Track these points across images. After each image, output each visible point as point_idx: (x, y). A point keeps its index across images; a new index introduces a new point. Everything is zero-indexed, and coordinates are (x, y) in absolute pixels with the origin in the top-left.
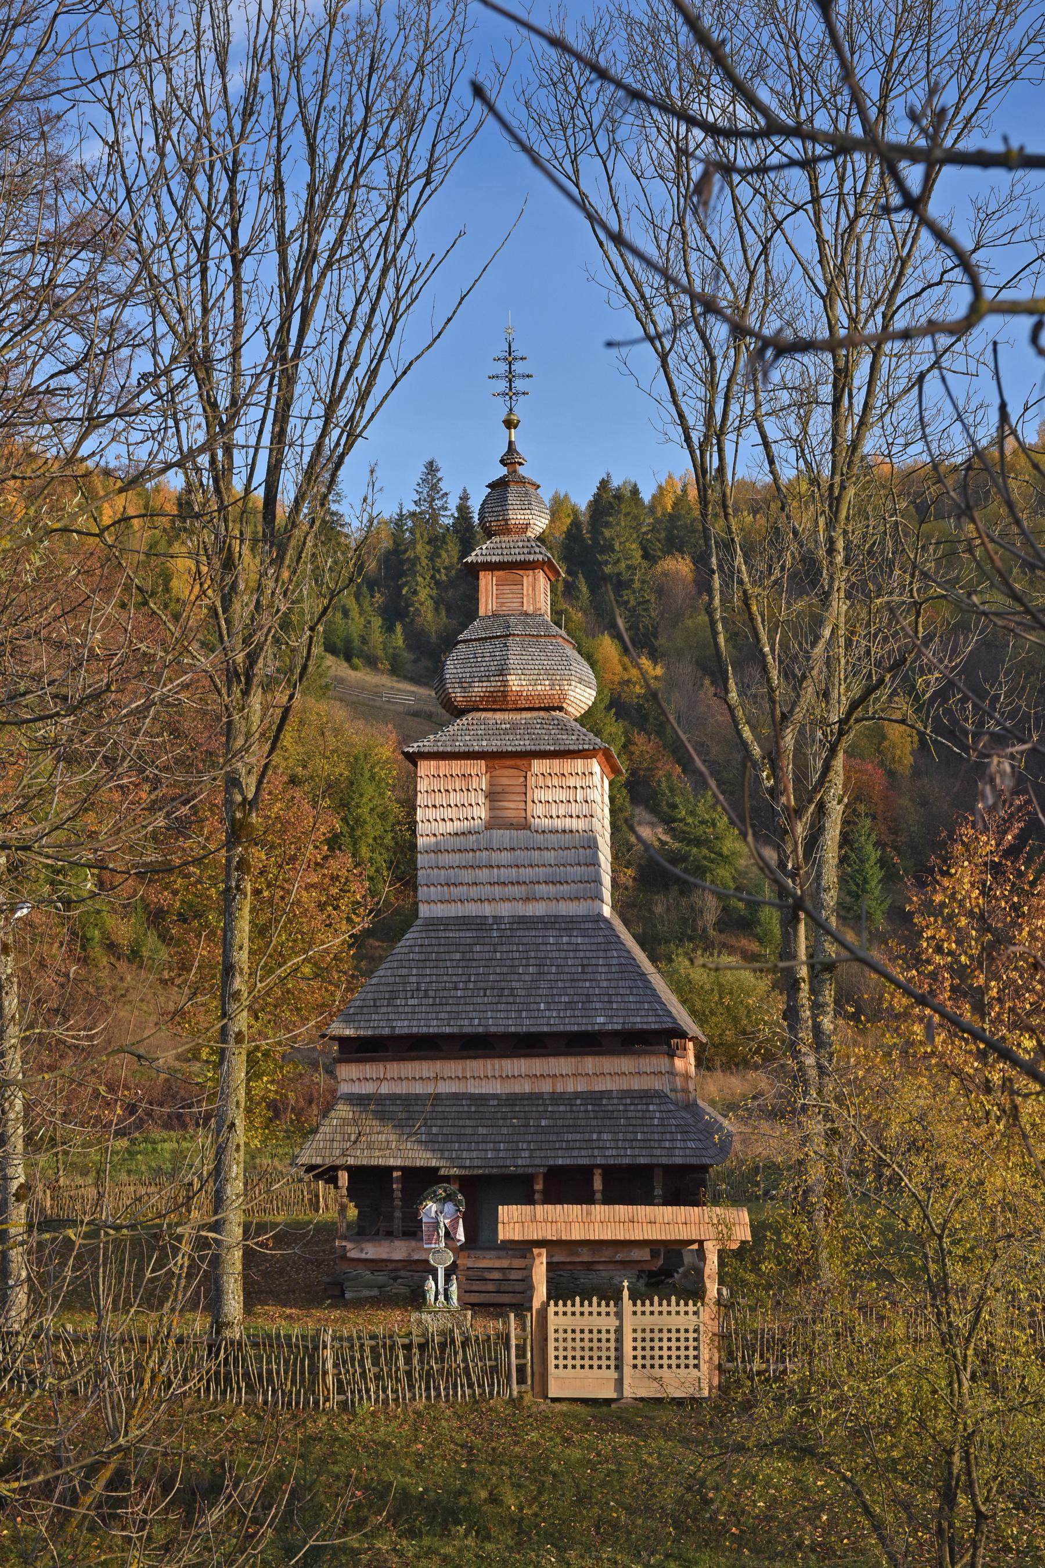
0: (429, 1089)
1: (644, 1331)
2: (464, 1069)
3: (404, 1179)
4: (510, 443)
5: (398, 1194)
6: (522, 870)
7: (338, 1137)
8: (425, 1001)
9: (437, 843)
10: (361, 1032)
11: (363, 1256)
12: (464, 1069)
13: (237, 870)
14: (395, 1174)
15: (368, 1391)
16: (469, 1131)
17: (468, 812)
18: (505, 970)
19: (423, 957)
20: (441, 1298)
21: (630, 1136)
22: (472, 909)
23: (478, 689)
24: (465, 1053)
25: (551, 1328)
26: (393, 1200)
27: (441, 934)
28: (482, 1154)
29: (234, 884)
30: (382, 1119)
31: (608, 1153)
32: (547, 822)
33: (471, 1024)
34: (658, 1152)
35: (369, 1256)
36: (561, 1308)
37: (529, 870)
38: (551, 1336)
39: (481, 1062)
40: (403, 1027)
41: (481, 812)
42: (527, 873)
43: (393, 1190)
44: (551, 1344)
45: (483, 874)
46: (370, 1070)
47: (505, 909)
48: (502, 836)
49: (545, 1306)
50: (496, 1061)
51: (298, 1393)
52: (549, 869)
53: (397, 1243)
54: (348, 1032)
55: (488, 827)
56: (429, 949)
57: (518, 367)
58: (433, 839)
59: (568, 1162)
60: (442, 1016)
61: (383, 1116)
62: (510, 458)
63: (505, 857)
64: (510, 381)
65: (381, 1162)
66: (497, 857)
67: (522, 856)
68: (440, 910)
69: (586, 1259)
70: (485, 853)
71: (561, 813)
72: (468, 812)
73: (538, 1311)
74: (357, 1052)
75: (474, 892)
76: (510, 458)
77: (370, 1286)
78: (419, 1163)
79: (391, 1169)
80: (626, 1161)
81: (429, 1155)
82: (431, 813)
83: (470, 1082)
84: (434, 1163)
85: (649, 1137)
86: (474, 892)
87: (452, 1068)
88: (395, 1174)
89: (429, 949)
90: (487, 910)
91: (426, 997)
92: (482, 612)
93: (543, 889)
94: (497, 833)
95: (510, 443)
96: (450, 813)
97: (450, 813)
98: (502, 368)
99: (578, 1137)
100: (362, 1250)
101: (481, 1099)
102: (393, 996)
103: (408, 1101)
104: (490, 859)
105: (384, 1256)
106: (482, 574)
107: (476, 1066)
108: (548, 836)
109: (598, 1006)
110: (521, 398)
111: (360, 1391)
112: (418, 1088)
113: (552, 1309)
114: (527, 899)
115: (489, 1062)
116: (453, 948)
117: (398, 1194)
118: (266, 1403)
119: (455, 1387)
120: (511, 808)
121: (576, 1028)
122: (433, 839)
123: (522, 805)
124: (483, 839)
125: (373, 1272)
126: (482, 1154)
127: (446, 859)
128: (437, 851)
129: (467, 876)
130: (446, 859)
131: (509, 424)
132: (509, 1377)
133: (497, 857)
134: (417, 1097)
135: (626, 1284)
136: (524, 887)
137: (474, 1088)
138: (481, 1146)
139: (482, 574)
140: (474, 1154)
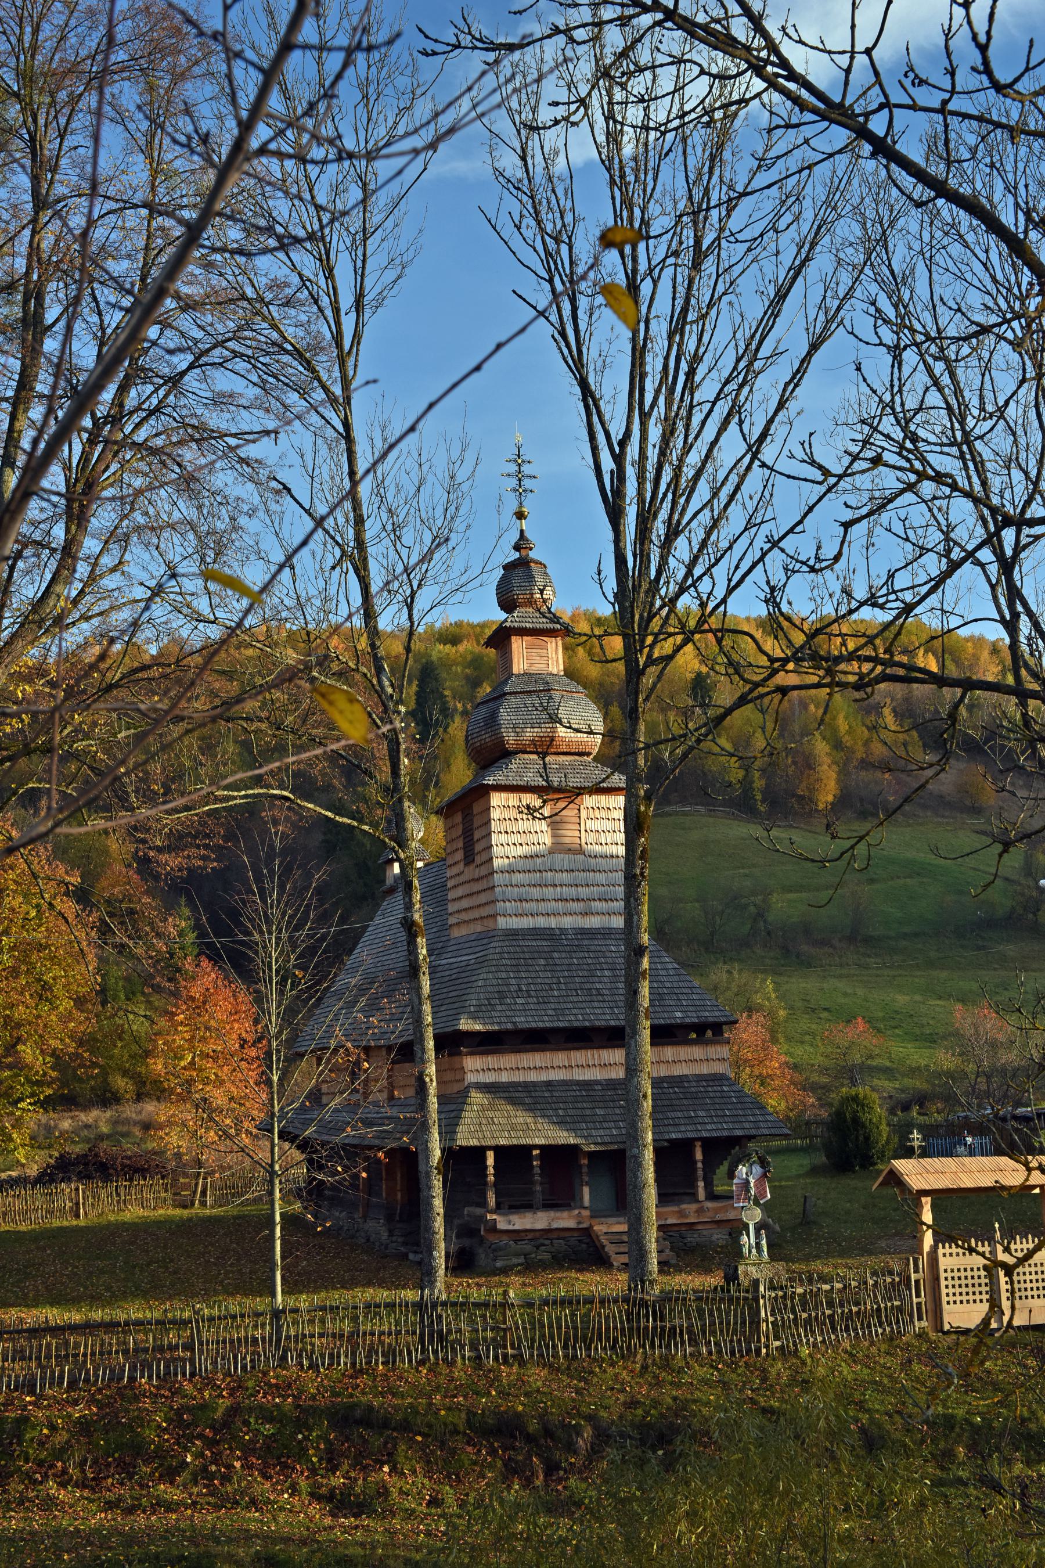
0: (543, 1077)
1: (972, 1270)
2: (569, 1059)
3: (541, 1157)
4: (522, 531)
5: (537, 1170)
6: (580, 889)
7: (484, 1121)
8: (530, 1000)
9: (510, 865)
10: (490, 1028)
11: (511, 1227)
12: (569, 1059)
13: (641, 858)
14: (536, 1152)
15: (799, 1335)
16: (588, 1112)
17: (533, 838)
18: (586, 973)
19: (514, 962)
20: (754, 1251)
21: (720, 1113)
22: (541, 922)
23: (530, 734)
24: (570, 1045)
25: (942, 1268)
26: (533, 1175)
27: (522, 943)
28: (608, 1132)
29: (638, 871)
30: (514, 1104)
31: (709, 1127)
32: (598, 848)
33: (576, 1018)
34: (746, 1125)
35: (516, 1227)
36: (947, 1251)
37: (586, 890)
38: (943, 1275)
39: (583, 1052)
40: (523, 1022)
41: (547, 839)
42: (584, 892)
43: (532, 1167)
44: (943, 1283)
45: (549, 892)
46: (492, 1061)
47: (568, 922)
48: (562, 860)
49: (934, 1249)
50: (595, 1051)
51: (739, 1341)
52: (601, 888)
53: (540, 1214)
54: (478, 1027)
55: (551, 851)
56: (516, 956)
57: (526, 469)
58: (506, 861)
59: (680, 1136)
60: (550, 1012)
61: (513, 1102)
62: (521, 544)
63: (566, 877)
64: (520, 480)
65: (523, 1142)
66: (559, 878)
67: (581, 876)
68: (514, 923)
69: (693, 1220)
70: (549, 874)
71: (609, 841)
72: (533, 838)
73: (928, 1254)
74: (478, 1046)
75: (542, 907)
76: (521, 544)
77: (517, 1255)
78: (561, 1141)
79: (531, 1147)
80: (725, 1134)
81: (566, 1134)
82: (504, 839)
83: (576, 1070)
84: (572, 1141)
85: (735, 1112)
86: (542, 907)
87: (560, 1058)
88: (536, 1152)
89: (516, 956)
90: (553, 922)
91: (530, 996)
92: (515, 671)
93: (597, 905)
94: (558, 857)
95: (522, 531)
96: (518, 839)
97: (518, 839)
98: (513, 468)
99: (679, 1114)
100: (509, 1222)
101: (587, 1085)
102: (502, 996)
103: (528, 1087)
104: (554, 878)
105: (528, 1227)
106: (513, 638)
107: (579, 1056)
108: (599, 860)
109: (672, 1003)
110: (529, 494)
111: (793, 1336)
112: (533, 1077)
113: (941, 1251)
114: (585, 914)
115: (589, 1052)
116: (536, 955)
117: (537, 1170)
118: (710, 1353)
119: (869, 1326)
120: (570, 835)
121: (662, 1022)
122: (506, 861)
123: (577, 834)
124: (547, 862)
125: (515, 1241)
126: (608, 1132)
127: (518, 878)
128: (510, 871)
129: (536, 893)
130: (518, 878)
131: (520, 515)
132: (911, 1316)
133: (559, 878)
134: (534, 1084)
135: (997, 1225)
136: (582, 904)
137: (579, 1075)
138: (605, 1125)
139: (513, 638)
140: (602, 1132)
